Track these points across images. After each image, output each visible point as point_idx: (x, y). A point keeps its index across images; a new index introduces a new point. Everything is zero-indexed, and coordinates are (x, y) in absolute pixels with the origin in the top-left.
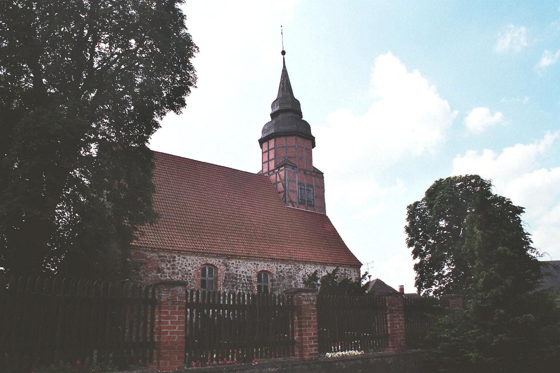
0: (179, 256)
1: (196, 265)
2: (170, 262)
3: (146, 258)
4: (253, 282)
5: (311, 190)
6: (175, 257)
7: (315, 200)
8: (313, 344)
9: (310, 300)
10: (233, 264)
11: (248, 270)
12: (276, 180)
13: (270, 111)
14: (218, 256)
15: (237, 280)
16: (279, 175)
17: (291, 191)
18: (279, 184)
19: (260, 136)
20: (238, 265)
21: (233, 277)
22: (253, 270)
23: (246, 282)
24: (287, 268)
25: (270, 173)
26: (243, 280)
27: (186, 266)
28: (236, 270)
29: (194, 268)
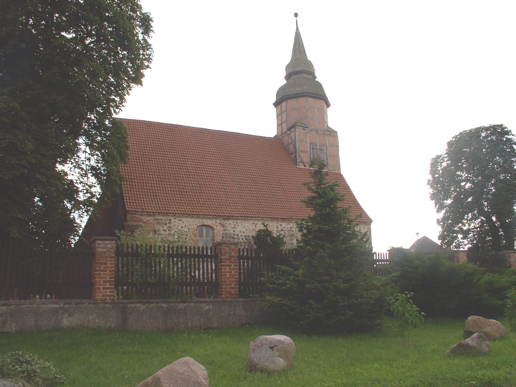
0: (175, 219)
1: (192, 227)
2: (166, 224)
3: (142, 221)
4: (251, 241)
5: (317, 149)
6: (170, 220)
7: (328, 159)
8: (108, 286)
9: (107, 248)
10: (231, 224)
11: (246, 229)
12: (289, 142)
13: (284, 74)
14: (215, 217)
15: (234, 239)
16: (290, 137)
17: (302, 151)
18: (291, 145)
19: (274, 100)
20: (235, 225)
21: (230, 237)
22: (251, 230)
23: (244, 241)
24: (288, 226)
25: (283, 135)
26: (240, 239)
27: (182, 227)
28: (233, 229)
29: (191, 229)
